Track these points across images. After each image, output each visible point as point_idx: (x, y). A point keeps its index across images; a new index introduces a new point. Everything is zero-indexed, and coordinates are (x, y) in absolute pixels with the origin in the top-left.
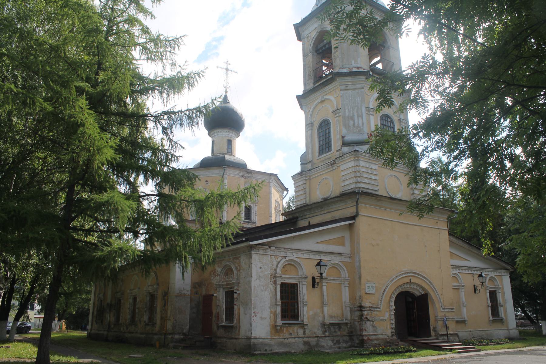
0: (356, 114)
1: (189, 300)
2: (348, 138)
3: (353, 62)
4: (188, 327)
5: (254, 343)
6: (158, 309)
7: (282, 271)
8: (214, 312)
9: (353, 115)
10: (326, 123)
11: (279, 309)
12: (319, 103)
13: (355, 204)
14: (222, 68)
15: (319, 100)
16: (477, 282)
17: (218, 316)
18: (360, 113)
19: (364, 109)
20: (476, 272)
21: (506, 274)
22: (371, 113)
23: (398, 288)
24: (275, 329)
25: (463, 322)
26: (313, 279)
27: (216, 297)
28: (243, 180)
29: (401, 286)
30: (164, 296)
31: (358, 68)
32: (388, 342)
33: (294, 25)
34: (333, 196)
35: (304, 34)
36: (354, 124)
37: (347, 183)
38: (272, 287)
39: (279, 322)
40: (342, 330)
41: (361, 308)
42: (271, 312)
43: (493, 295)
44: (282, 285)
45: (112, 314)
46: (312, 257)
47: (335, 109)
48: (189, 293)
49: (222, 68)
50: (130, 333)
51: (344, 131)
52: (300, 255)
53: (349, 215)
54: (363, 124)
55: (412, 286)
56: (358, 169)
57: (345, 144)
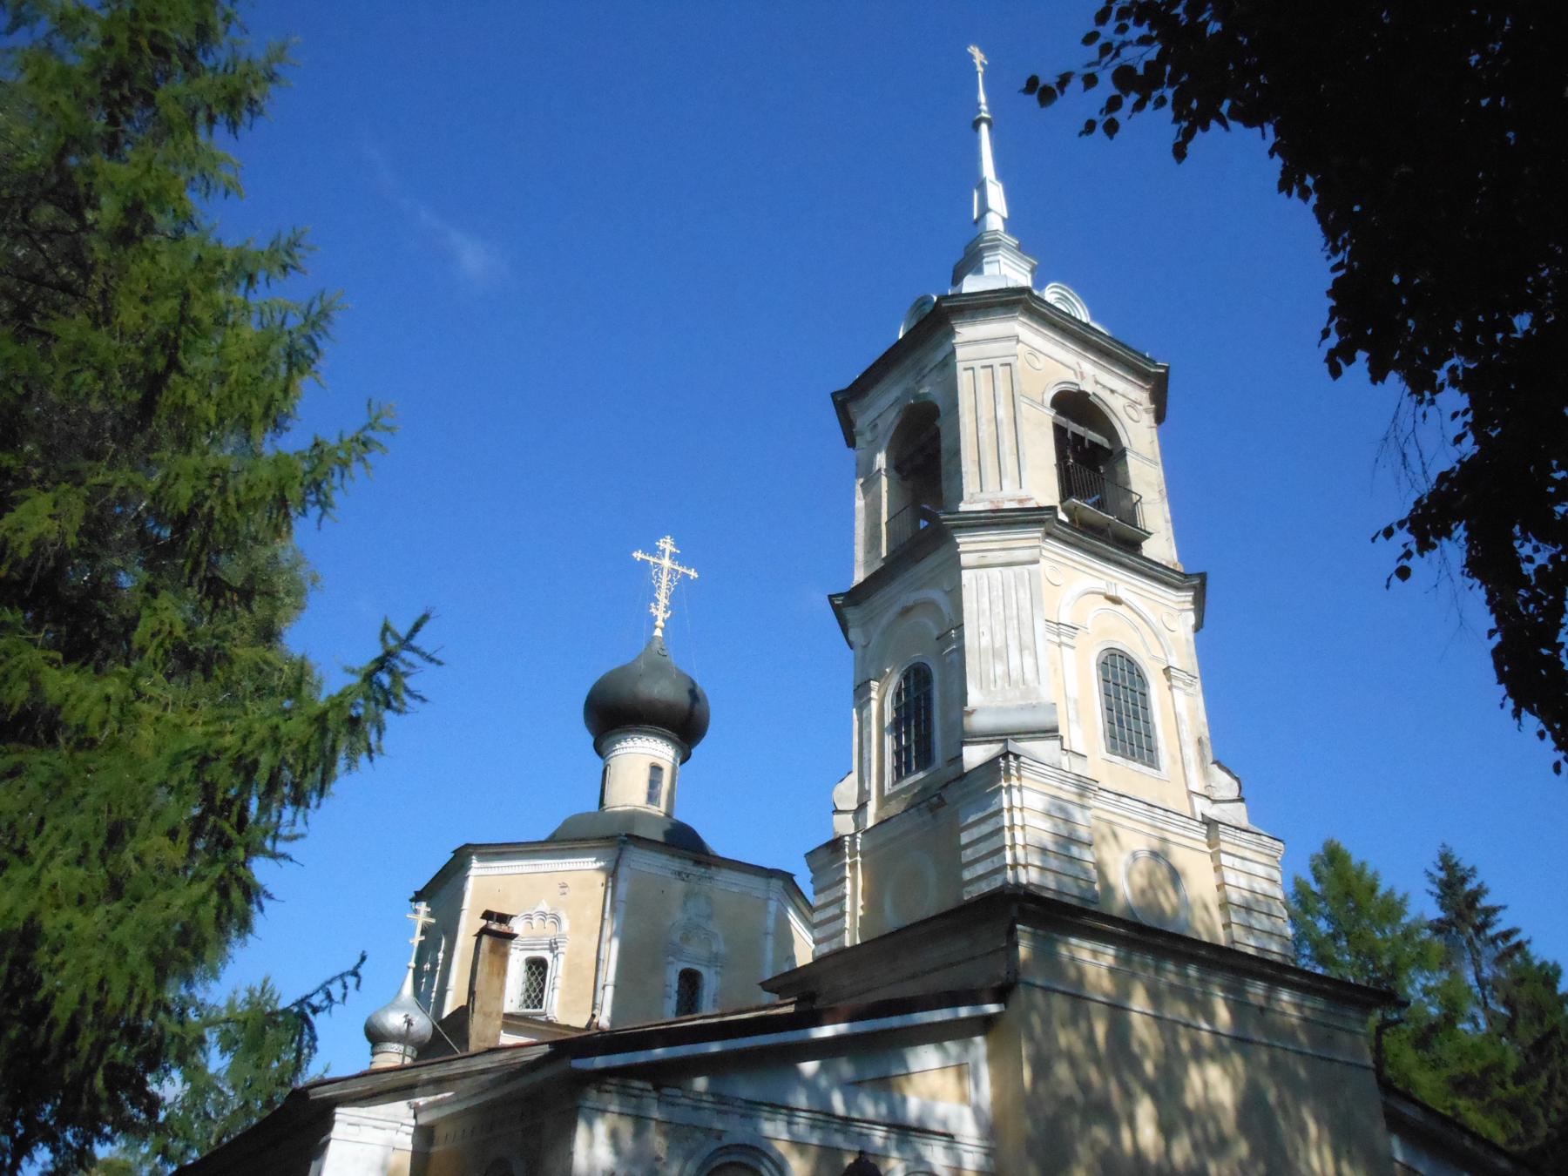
15: (897, 608)
22: (1064, 639)
28: (679, 886)
33: (834, 395)
35: (861, 422)
40: (244, 834)
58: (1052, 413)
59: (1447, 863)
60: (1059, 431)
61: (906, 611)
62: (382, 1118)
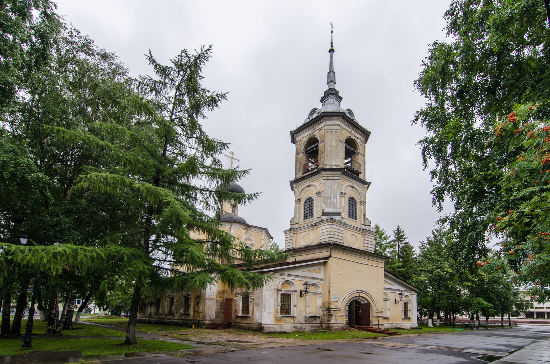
0: (332, 196)
1: (215, 301)
2: (327, 210)
3: (334, 162)
4: (214, 317)
5: (263, 327)
6: (192, 306)
7: (282, 287)
8: (234, 309)
9: (331, 197)
10: (311, 200)
11: (279, 308)
12: (306, 187)
13: (329, 250)
14: (228, 157)
16: (398, 297)
17: (236, 311)
18: (335, 196)
19: (338, 193)
20: (397, 292)
21: (415, 294)
23: (352, 298)
24: (278, 319)
25: (387, 318)
26: (301, 292)
27: (236, 300)
29: (353, 298)
30: (197, 299)
31: (337, 166)
32: (344, 328)
33: (291, 132)
34: (312, 244)
35: (298, 139)
36: (331, 202)
37: (323, 237)
38: (275, 295)
39: (279, 315)
41: (329, 309)
42: (274, 310)
43: (406, 305)
44: (282, 294)
45: (152, 308)
46: (300, 279)
47: (318, 192)
48: (215, 297)
49: (228, 157)
50: (168, 319)
51: (324, 206)
52: (293, 278)
53: (324, 256)
54: (337, 202)
55: (360, 298)
56: (332, 230)
57: (324, 214)
58: (345, 144)
59: (398, 230)
60: (346, 147)
61: (308, 186)
62: (231, 343)
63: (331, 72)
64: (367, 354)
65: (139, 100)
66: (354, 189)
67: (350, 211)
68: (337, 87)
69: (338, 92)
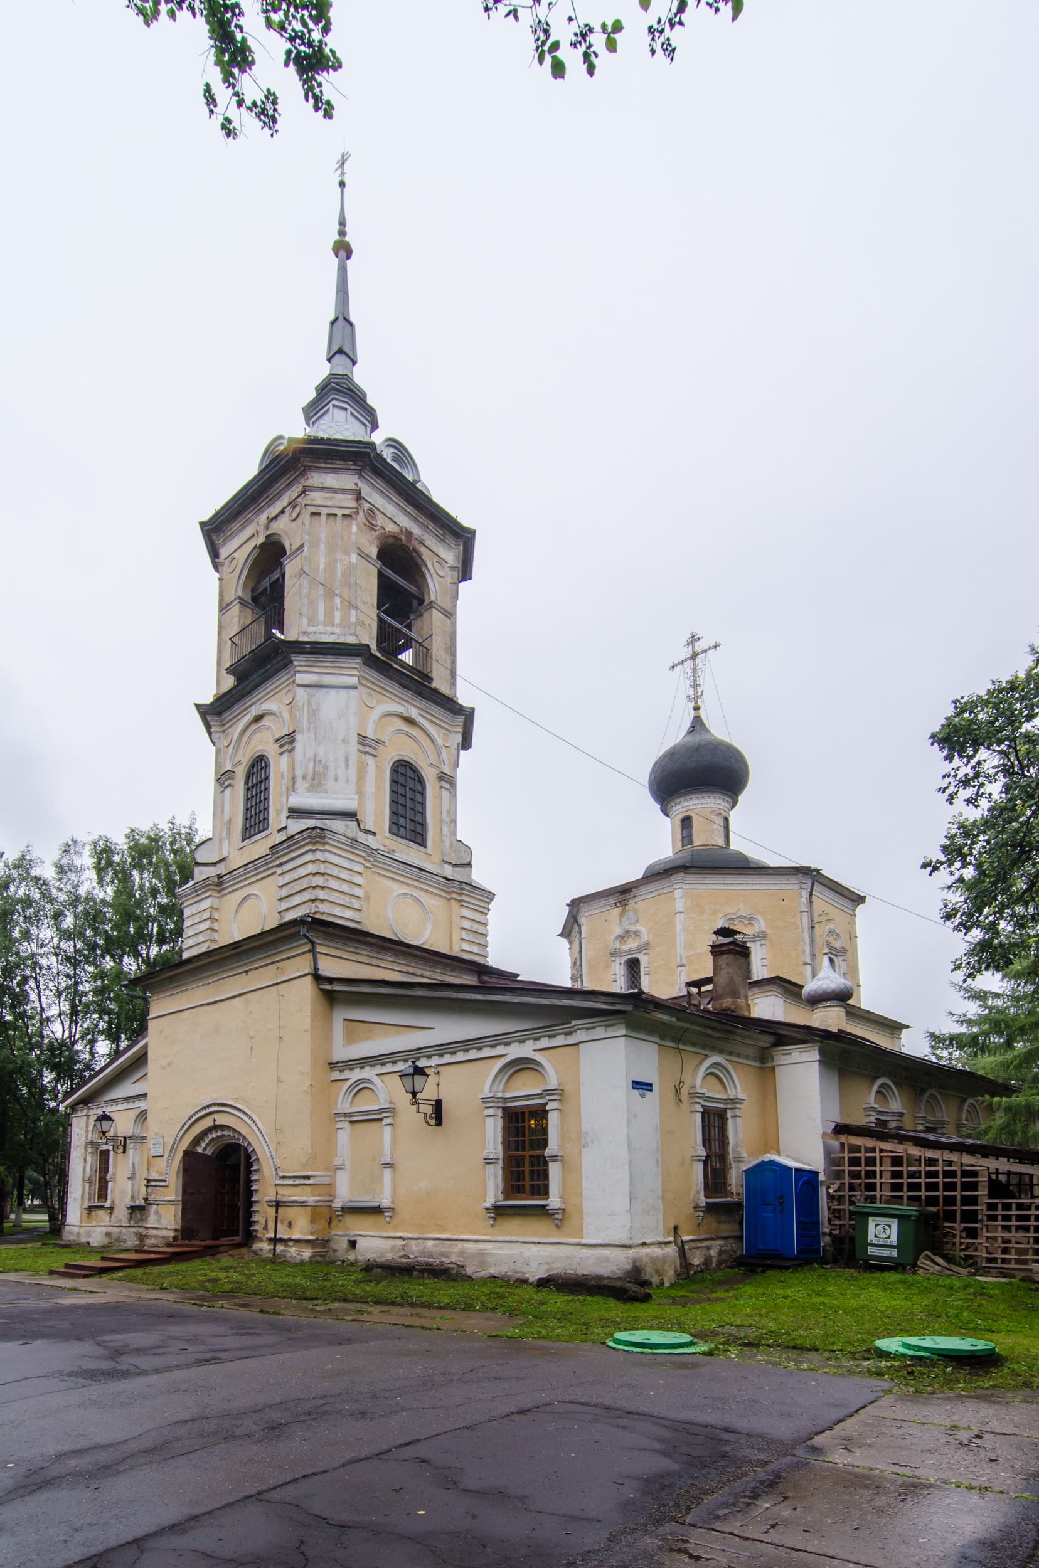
58: (379, 564)
60: (381, 575)
63: (342, 322)
64: (363, 965)
65: (176, 957)
66: (414, 731)
67: (402, 821)
68: (361, 376)
69: (365, 395)
